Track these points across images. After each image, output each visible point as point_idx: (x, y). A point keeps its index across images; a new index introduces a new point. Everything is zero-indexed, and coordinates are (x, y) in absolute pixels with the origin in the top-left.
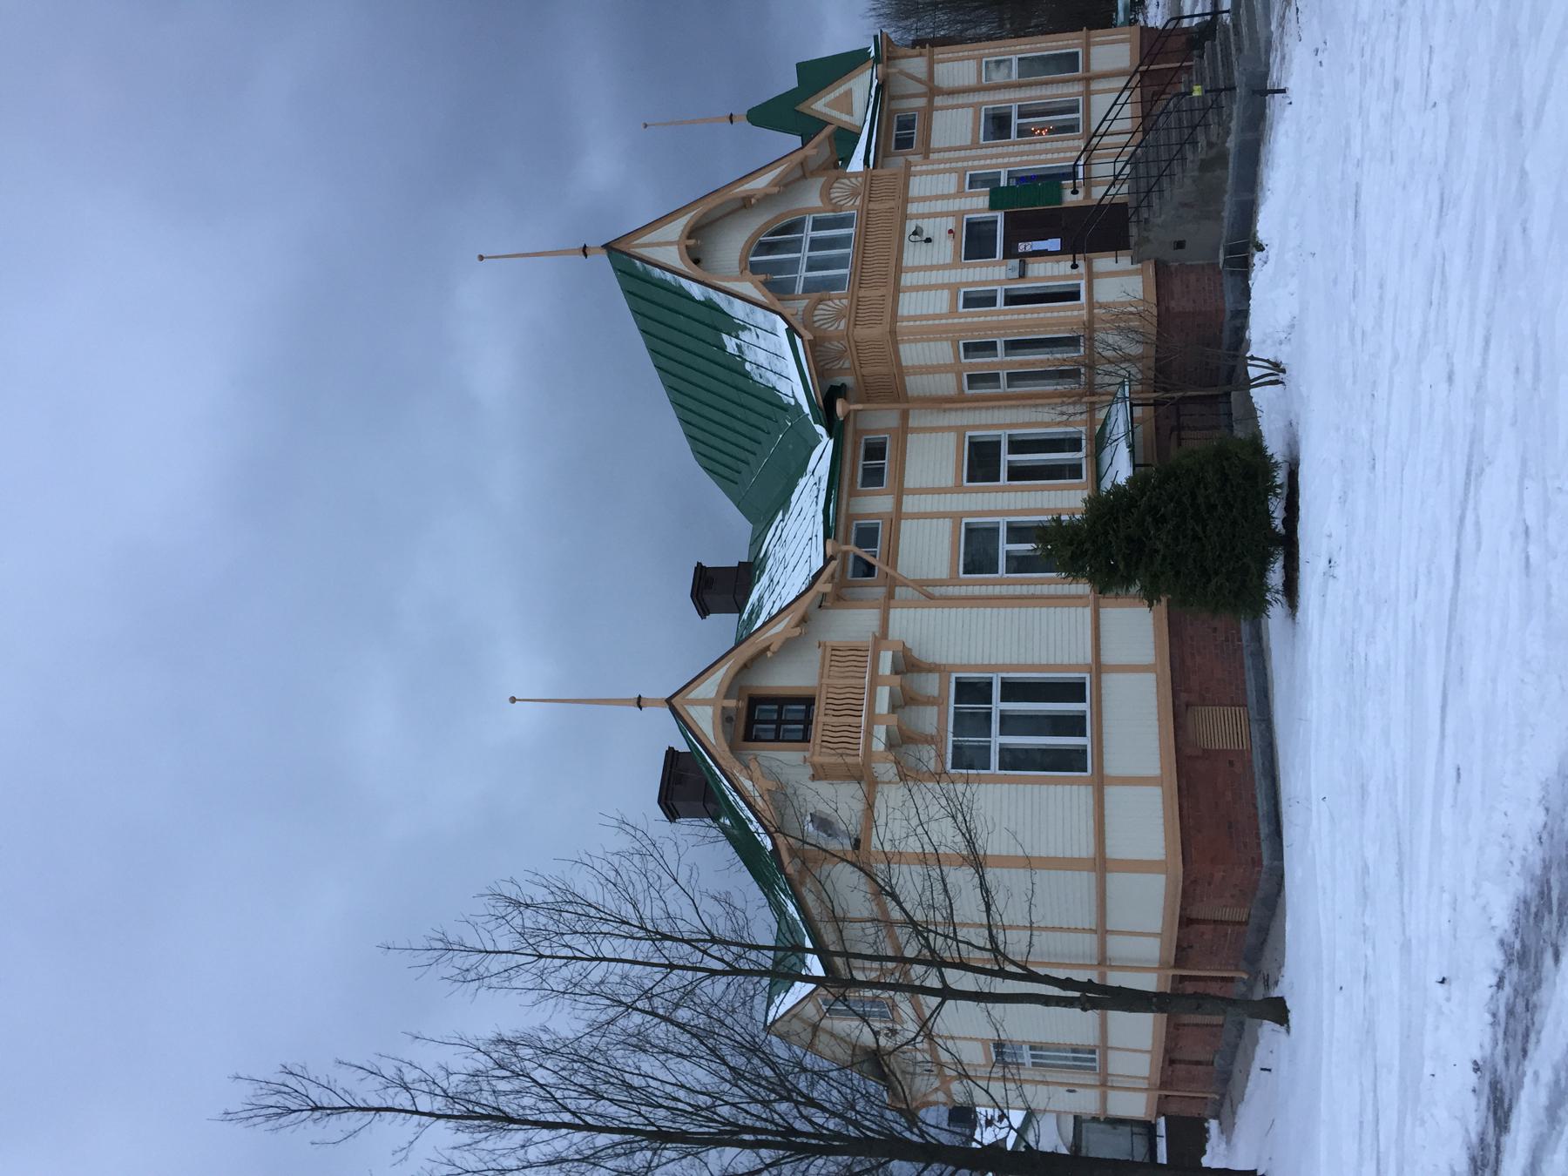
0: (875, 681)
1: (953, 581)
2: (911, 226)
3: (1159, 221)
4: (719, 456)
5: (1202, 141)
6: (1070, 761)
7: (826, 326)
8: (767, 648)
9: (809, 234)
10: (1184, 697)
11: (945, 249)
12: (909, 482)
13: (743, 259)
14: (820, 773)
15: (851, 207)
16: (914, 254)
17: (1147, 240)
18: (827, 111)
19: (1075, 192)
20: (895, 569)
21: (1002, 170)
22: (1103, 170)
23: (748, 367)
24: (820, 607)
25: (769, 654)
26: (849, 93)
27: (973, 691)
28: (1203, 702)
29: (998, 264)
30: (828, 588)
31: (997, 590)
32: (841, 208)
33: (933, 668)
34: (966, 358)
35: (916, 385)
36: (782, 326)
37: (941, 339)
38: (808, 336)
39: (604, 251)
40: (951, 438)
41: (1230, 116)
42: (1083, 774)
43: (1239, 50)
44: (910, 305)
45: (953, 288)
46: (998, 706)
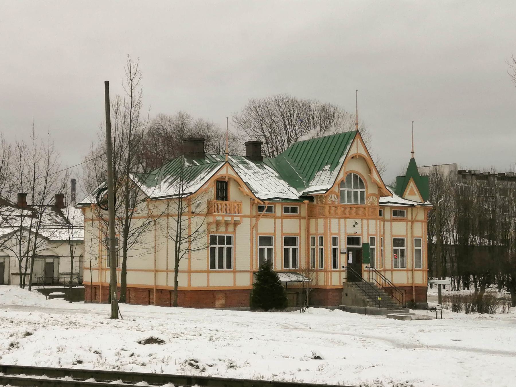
0: (232, 216)
1: (257, 234)
2: (359, 221)
3: (352, 290)
4: (298, 150)
5: (368, 300)
6: (213, 266)
7: (329, 198)
8: (240, 186)
9: (359, 190)
10: (228, 292)
11: (351, 231)
12: (284, 220)
13: (352, 171)
14: (209, 202)
15: (367, 202)
16: (350, 222)
17: (348, 286)
18: (410, 186)
19: (366, 267)
20: (261, 218)
21: (375, 246)
22: (373, 275)
23: (321, 172)
24: (251, 199)
25: (239, 187)
26: (415, 194)
27: (229, 241)
28: (226, 297)
29: (345, 246)
30: (256, 202)
31: (254, 246)
32: (367, 200)
33: (235, 229)
34: (320, 237)
35: (313, 221)
36: (329, 187)
37: (324, 231)
38: (325, 195)
39: (356, 130)
40: (297, 232)
41: (374, 307)
42: (210, 268)
43: (388, 309)
44: (334, 222)
45: (339, 234)
46: (225, 247)
